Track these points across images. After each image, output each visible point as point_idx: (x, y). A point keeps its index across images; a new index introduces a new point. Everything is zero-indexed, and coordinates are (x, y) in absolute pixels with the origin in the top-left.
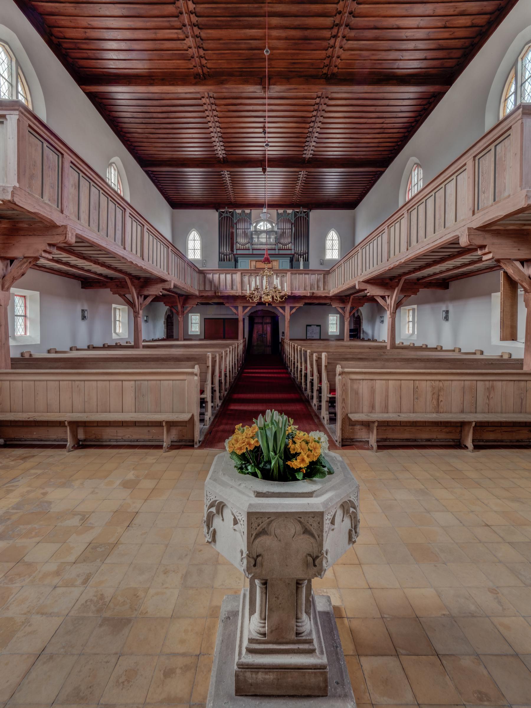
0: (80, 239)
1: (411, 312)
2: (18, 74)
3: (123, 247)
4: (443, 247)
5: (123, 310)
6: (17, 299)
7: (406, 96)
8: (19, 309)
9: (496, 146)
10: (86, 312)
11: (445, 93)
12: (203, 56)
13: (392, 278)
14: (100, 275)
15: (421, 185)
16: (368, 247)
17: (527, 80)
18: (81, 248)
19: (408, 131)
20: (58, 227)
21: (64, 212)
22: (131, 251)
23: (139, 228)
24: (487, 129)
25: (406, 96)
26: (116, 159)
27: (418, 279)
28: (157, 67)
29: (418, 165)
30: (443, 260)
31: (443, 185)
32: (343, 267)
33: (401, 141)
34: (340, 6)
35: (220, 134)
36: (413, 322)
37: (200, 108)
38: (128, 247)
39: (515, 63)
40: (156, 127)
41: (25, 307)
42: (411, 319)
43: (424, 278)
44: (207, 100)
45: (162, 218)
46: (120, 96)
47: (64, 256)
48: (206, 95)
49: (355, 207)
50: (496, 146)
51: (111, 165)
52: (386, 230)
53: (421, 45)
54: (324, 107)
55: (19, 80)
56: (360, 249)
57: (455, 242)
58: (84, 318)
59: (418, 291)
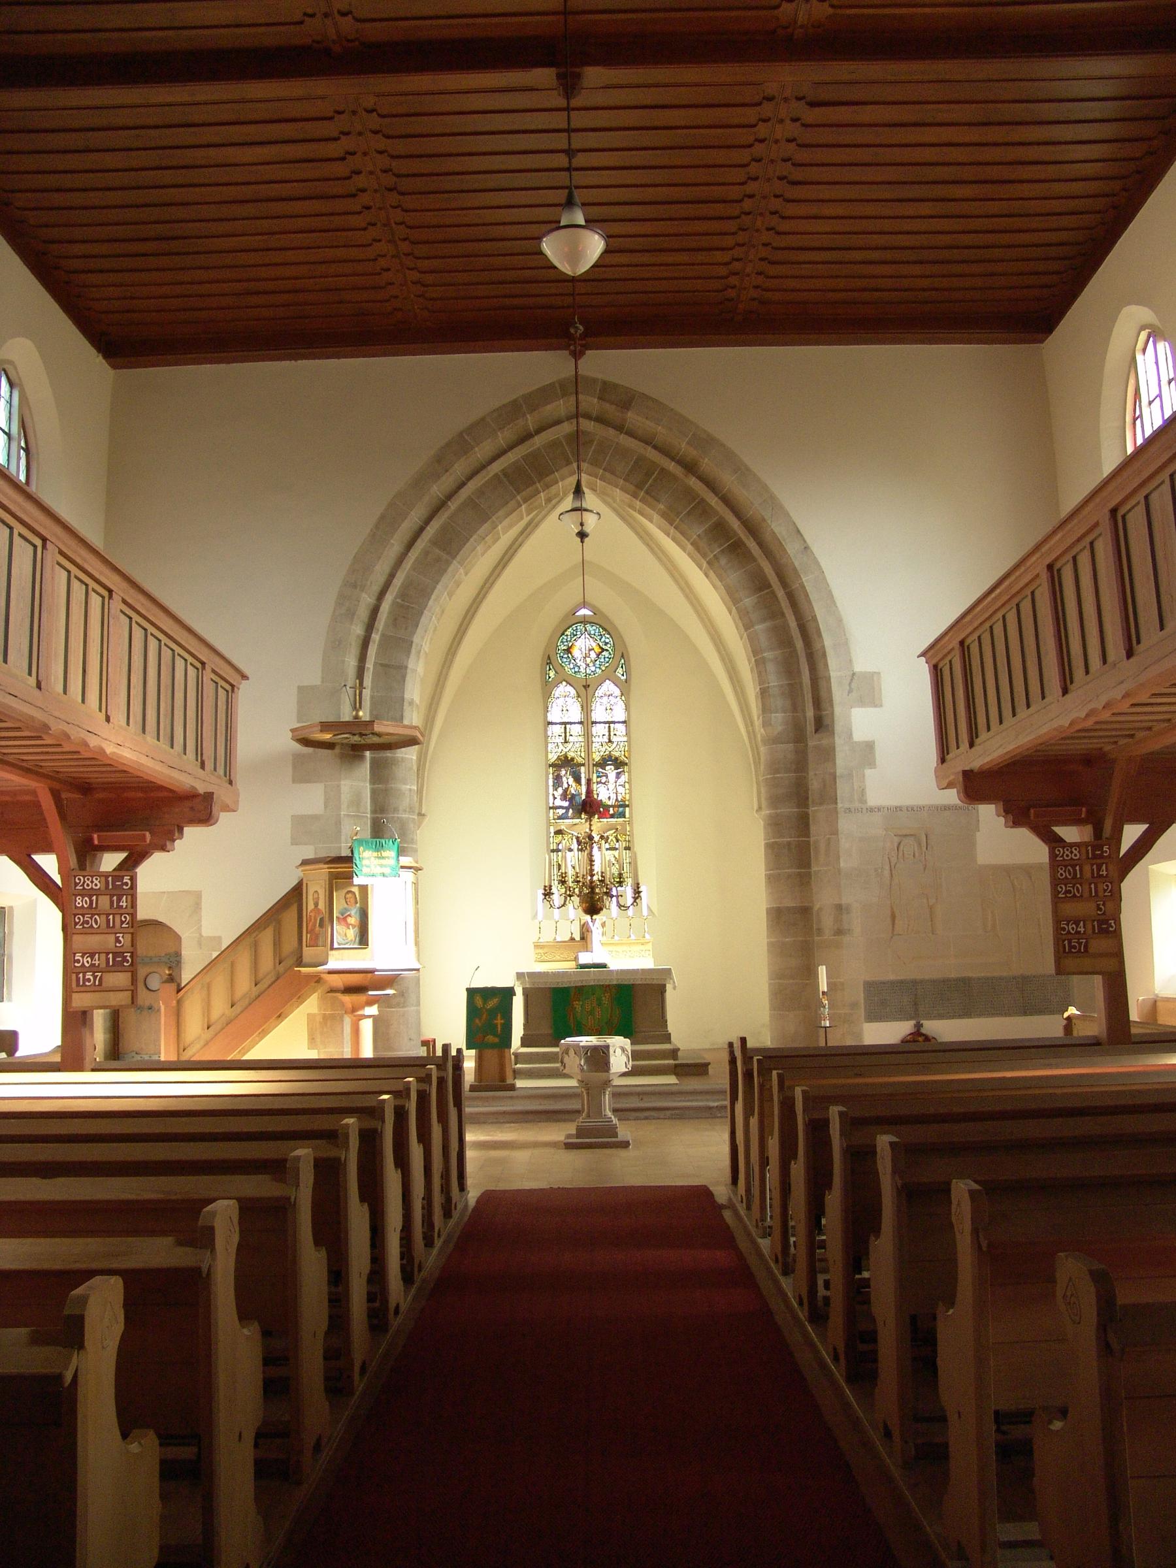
3: (32, 681)
23: (192, 672)
29: (1156, 334)
35: (374, 121)
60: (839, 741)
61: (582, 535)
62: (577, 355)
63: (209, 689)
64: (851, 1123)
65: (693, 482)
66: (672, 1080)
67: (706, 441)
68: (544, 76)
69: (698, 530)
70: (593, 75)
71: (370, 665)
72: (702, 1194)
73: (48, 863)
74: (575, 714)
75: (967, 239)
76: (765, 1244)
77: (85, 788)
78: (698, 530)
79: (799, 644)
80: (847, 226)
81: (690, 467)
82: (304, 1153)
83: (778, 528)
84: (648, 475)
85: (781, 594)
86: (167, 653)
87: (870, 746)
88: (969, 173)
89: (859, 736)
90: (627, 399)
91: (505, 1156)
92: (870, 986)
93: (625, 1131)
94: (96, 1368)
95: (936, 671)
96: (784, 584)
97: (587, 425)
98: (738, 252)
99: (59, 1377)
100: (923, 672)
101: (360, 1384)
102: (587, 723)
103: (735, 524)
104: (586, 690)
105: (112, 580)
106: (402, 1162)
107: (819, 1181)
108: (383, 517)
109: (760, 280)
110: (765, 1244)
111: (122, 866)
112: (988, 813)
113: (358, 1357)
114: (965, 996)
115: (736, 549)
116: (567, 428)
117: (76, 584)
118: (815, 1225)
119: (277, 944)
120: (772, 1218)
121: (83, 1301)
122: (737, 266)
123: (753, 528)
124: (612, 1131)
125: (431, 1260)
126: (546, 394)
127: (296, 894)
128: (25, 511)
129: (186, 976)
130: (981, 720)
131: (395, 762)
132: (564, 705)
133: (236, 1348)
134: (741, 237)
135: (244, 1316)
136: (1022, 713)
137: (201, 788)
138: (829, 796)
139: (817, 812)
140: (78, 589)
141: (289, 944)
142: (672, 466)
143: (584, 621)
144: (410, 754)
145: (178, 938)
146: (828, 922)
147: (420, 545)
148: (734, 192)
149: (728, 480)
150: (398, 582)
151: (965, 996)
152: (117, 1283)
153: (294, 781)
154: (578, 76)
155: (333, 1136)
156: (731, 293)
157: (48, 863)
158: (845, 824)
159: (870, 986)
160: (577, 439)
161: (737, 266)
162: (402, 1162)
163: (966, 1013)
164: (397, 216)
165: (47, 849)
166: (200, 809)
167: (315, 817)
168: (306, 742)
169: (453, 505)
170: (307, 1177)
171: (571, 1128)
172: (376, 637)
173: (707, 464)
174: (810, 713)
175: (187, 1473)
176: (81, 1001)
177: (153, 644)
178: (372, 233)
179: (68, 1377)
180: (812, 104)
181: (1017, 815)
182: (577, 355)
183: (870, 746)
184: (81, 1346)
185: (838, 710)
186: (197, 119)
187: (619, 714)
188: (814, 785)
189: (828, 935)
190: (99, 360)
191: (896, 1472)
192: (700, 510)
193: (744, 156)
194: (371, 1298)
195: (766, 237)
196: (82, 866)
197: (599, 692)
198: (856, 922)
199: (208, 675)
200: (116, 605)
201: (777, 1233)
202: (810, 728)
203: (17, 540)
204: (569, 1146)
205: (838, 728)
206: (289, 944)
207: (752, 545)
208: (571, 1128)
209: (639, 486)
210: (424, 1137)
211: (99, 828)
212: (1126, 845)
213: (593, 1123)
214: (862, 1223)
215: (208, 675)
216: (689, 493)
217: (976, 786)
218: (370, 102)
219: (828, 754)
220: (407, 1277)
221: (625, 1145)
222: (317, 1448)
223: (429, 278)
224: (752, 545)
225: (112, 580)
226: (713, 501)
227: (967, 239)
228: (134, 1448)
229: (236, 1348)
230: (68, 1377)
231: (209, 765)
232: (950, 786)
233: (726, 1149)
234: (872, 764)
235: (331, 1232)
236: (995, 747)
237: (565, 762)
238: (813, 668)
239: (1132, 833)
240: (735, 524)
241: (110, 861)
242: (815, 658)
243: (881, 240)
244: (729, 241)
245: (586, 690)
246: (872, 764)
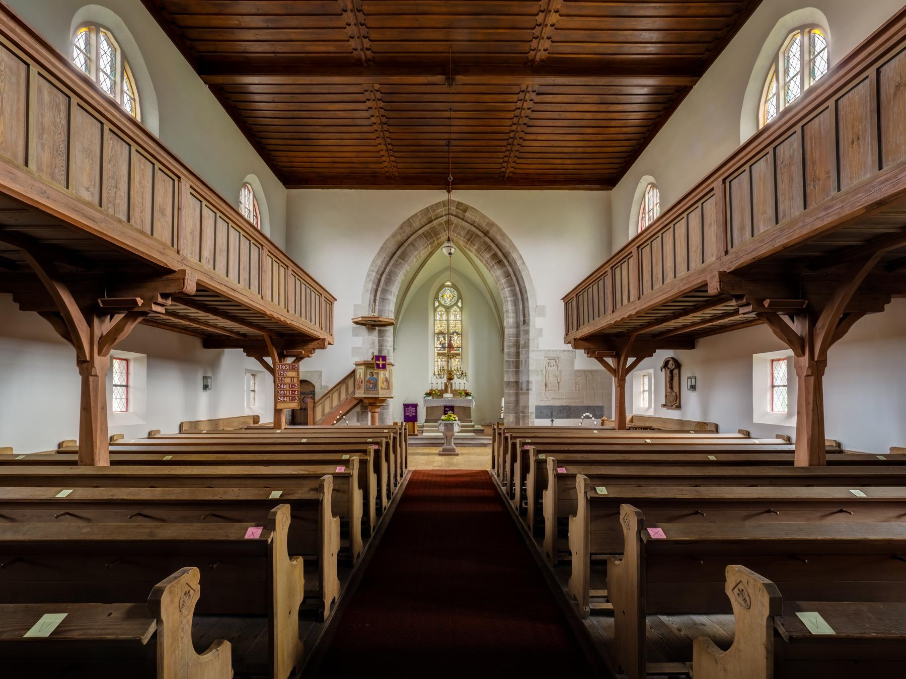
0: (202, 288)
1: (646, 380)
2: (123, 69)
3: (260, 296)
4: (686, 295)
5: (135, 359)
6: (116, 363)
7: (640, 89)
8: (118, 378)
9: (803, 127)
10: (209, 380)
11: (692, 87)
12: (363, 22)
13: (618, 335)
14: (231, 331)
15: (657, 212)
16: (595, 287)
17: (819, 54)
18: (207, 299)
19: (665, 108)
20: (172, 272)
21: (181, 252)
22: (129, 221)
23: (317, 297)
24: (744, 140)
25: (640, 89)
26: (251, 178)
27: (662, 333)
28: (302, 51)
29: (654, 186)
30: (686, 312)
31: (649, 242)
32: (608, 280)
33: (708, 50)
34: (543, 4)
35: (379, 95)
36: (650, 391)
37: (376, 154)
38: (292, 311)
39: (775, 59)
40: (291, 108)
41: (127, 374)
42: (646, 388)
43: (669, 331)
44: (358, 41)
45: (255, 195)
46: (253, 89)
47: (181, 308)
48: (350, 7)
49: (614, 185)
50: (775, 148)
51: (244, 185)
52: (610, 272)
53: (655, 36)
54: (522, 135)
55: (125, 77)
56: (609, 269)
57: (703, 287)
58: (206, 387)
59: (889, 302)
60: (531, 328)
61: (450, 254)
62: (449, 192)
63: (323, 303)
64: (512, 438)
65: (487, 239)
66: (473, 434)
67: (492, 224)
68: (439, 78)
69: (487, 256)
70: (460, 78)
71: (378, 298)
72: (485, 472)
73: (269, 360)
74: (444, 317)
75: (589, 150)
76: (504, 489)
77: (281, 335)
78: (487, 256)
79: (519, 296)
80: (545, 143)
81: (486, 234)
82: (356, 458)
83: (514, 255)
84: (472, 236)
85: (514, 278)
86: (308, 290)
87: (541, 330)
88: (592, 123)
89: (537, 326)
90: (465, 209)
91: (423, 461)
92: (537, 407)
93: (458, 450)
94: (280, 538)
95: (566, 304)
96: (515, 275)
97: (452, 218)
98: (507, 153)
99: (267, 541)
100: (562, 304)
101: (372, 534)
102: (448, 320)
103: (500, 254)
104: (448, 309)
105: (321, 291)
106: (388, 460)
107: (514, 460)
108: (382, 248)
109: (514, 165)
110: (504, 489)
111: (294, 362)
112: (580, 353)
113: (372, 525)
114: (568, 411)
115: (500, 262)
116: (445, 218)
117: (275, 263)
118: (523, 483)
119: (347, 389)
120: (508, 482)
121: (275, 513)
122: (506, 159)
123: (506, 256)
124: (454, 450)
125: (398, 491)
126: (438, 205)
127: (354, 372)
128: (13, 31)
129: (317, 398)
130: (581, 322)
131: (386, 331)
132: (441, 315)
133: (331, 526)
134: (509, 148)
135: (334, 515)
136: (597, 319)
137: (321, 337)
138: (527, 346)
139: (522, 352)
140: (298, 283)
141: (351, 390)
142: (480, 233)
143: (448, 286)
144: (391, 328)
145: (314, 386)
146: (524, 386)
147: (395, 258)
148: (507, 129)
149: (499, 238)
150: (387, 271)
151: (568, 411)
152: (288, 506)
153: (353, 335)
154: (453, 79)
155: (365, 452)
156: (503, 170)
157: (269, 360)
158: (532, 355)
159: (537, 407)
160: (448, 223)
161: (506, 159)
162: (388, 460)
163: (568, 417)
164: (387, 134)
165: (268, 355)
166: (322, 344)
167: (360, 348)
168: (357, 323)
169: (406, 244)
170: (356, 466)
171: (441, 449)
172: (380, 289)
173: (492, 232)
174: (522, 319)
175: (313, 568)
176: (280, 406)
177: (303, 286)
178: (378, 141)
179: (270, 540)
180: (538, 94)
181: (590, 353)
182: (449, 192)
183: (541, 330)
184: (274, 530)
185: (531, 318)
186: (313, 91)
187: (459, 318)
188: (522, 342)
189: (524, 390)
190: (280, 184)
191: (552, 569)
192: (489, 249)
193: (511, 115)
194: (377, 504)
195: (518, 147)
196: (280, 361)
197: (452, 310)
198: (534, 387)
199: (323, 299)
200: (290, 272)
201: (509, 484)
202: (521, 323)
203: (231, 230)
204: (440, 455)
205: (531, 324)
206: (351, 390)
207: (505, 261)
208: (441, 449)
209: (468, 240)
210: (395, 452)
211: (285, 349)
212: (628, 365)
213: (448, 447)
214: (514, 460)
215: (323, 299)
216: (485, 243)
217: (578, 343)
218: (377, 87)
219: (527, 332)
220: (389, 497)
221: (457, 455)
222: (358, 555)
223: (398, 160)
224: (505, 261)
225: (321, 291)
226: (493, 246)
227: (589, 150)
228: (295, 562)
229: (331, 526)
230: (270, 540)
231: (324, 329)
232: (569, 343)
233: (490, 457)
234: (541, 336)
235: (364, 485)
236: (586, 330)
237: (441, 333)
238: (523, 304)
239: (631, 360)
240: (500, 254)
241: (290, 360)
242: (524, 300)
243: (559, 150)
244: (504, 149)
245: (448, 309)
246: (541, 336)
